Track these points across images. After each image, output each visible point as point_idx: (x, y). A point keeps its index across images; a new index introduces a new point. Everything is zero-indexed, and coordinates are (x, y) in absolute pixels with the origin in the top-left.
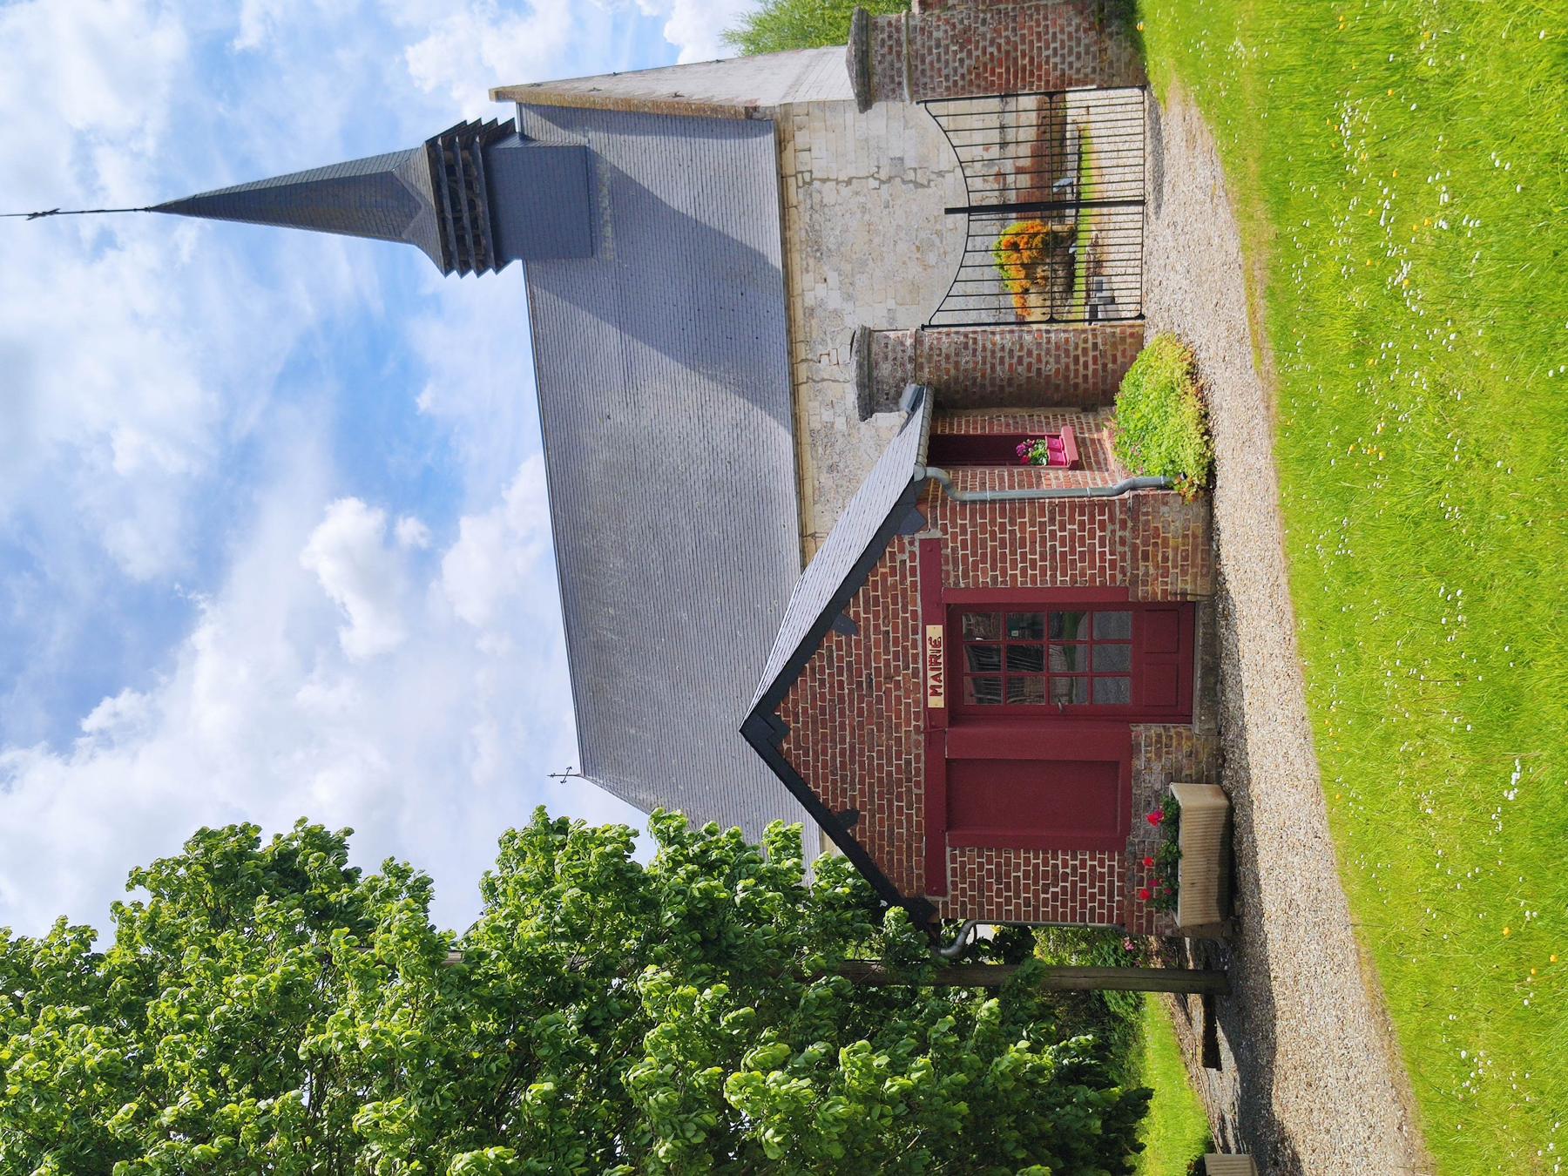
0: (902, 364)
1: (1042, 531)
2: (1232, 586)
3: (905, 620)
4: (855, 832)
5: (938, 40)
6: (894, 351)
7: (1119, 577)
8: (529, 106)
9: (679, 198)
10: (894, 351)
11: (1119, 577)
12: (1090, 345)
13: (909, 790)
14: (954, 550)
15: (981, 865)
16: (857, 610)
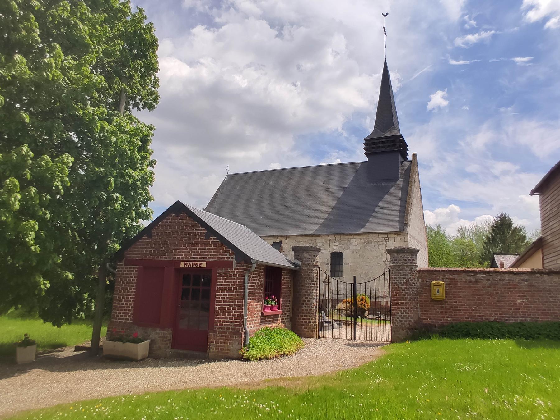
0: (307, 261)
1: (233, 302)
2: (212, 364)
3: (208, 255)
4: (145, 237)
5: (408, 275)
6: (312, 258)
7: (217, 327)
8: (411, 164)
9: (382, 205)
10: (312, 258)
11: (217, 327)
12: (310, 321)
13: (156, 255)
14: (229, 272)
15: (132, 277)
16: (213, 239)
